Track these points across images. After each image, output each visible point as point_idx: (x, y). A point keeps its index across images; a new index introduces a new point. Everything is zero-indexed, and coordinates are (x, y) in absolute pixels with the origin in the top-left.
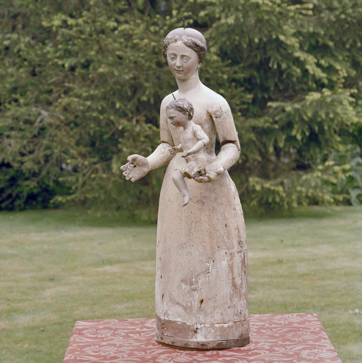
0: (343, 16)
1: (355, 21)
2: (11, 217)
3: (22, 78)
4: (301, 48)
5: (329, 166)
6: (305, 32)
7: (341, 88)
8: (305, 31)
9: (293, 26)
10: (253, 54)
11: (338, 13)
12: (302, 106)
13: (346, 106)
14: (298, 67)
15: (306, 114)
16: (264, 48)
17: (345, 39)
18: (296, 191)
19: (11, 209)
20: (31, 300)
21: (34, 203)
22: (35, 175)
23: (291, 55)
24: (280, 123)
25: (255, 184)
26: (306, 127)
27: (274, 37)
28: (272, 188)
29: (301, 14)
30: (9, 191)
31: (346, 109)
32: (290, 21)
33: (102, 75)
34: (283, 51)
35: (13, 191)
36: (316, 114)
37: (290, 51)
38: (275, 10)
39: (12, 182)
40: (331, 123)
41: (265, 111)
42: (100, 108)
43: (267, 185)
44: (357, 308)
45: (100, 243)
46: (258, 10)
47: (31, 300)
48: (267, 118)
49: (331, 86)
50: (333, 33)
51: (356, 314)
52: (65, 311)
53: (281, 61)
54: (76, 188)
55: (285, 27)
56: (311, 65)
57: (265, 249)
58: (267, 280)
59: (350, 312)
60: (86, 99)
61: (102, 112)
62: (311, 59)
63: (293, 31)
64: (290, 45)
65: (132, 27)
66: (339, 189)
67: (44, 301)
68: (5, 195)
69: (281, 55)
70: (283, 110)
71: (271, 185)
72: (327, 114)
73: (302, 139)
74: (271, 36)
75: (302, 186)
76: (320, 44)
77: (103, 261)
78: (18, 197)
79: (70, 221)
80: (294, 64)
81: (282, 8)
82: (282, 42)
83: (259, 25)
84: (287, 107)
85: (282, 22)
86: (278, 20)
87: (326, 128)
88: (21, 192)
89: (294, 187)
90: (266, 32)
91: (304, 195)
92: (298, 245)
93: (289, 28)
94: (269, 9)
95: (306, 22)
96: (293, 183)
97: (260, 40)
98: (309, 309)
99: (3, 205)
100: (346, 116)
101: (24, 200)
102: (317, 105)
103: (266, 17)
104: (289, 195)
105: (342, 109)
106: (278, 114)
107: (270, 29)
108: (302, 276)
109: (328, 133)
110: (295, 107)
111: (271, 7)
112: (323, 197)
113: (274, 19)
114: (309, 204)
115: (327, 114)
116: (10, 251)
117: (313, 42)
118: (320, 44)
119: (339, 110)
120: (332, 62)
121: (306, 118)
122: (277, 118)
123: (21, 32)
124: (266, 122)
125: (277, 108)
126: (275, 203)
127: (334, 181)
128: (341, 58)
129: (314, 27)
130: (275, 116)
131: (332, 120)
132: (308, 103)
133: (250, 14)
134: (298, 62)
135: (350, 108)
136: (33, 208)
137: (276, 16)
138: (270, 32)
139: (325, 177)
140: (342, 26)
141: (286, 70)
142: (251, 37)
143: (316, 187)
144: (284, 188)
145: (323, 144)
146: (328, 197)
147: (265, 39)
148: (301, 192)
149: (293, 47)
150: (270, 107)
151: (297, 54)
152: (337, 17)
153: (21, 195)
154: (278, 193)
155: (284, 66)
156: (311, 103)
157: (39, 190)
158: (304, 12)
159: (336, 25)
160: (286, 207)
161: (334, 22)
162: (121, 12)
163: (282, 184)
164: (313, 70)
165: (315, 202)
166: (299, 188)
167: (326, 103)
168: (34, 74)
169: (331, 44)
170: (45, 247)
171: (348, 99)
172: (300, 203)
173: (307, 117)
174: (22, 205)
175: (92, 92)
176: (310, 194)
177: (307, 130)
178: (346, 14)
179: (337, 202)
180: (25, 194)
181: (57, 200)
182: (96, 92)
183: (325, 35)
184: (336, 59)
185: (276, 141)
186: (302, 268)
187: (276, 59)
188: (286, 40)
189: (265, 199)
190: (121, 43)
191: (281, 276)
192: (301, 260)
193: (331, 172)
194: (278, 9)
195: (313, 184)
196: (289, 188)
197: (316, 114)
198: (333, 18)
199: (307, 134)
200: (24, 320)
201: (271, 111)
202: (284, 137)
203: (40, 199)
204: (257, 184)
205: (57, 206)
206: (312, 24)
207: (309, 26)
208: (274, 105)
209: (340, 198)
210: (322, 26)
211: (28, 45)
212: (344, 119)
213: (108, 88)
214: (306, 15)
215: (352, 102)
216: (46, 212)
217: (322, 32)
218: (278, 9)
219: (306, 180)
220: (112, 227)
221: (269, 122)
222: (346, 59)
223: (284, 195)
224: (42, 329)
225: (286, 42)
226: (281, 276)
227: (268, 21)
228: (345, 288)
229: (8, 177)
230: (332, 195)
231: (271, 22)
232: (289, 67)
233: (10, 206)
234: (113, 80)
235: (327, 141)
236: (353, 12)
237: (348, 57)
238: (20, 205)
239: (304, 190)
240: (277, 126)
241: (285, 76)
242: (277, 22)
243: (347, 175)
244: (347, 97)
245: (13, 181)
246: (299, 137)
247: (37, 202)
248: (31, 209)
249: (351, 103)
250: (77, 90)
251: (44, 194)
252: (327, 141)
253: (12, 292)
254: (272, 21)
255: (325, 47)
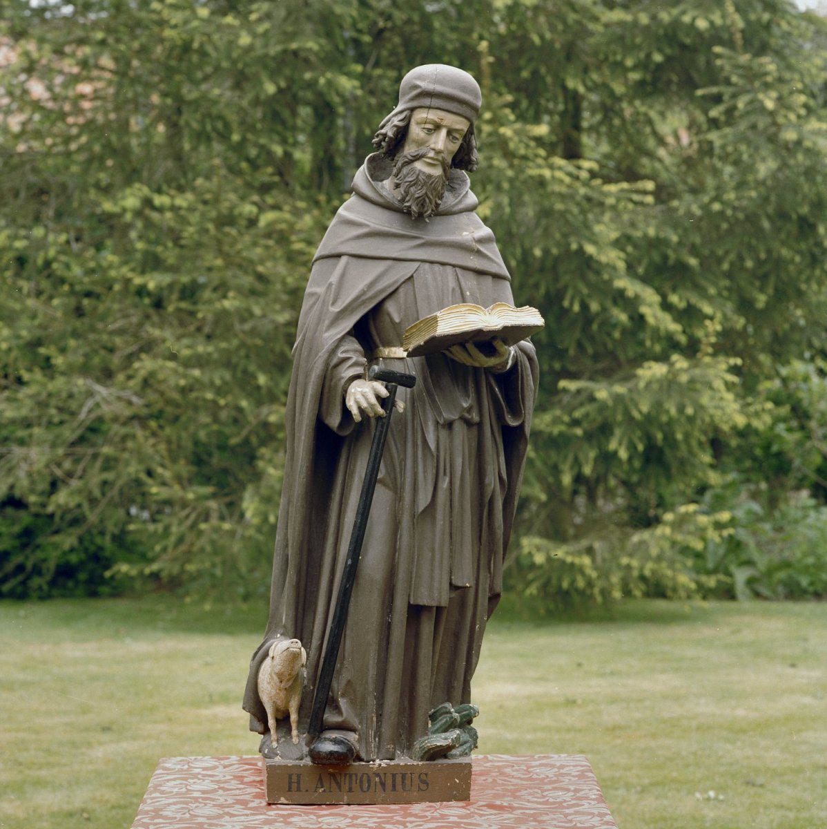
0: (716, 207)
1: (741, 216)
2: (22, 613)
3: (54, 319)
4: (631, 268)
5: (687, 514)
6: (639, 238)
7: (708, 354)
8: (638, 234)
9: (613, 226)
10: (531, 281)
11: (706, 199)
12: (630, 390)
13: (719, 391)
14: (625, 310)
15: (636, 406)
16: (554, 268)
17: (720, 252)
18: (619, 566)
19: (20, 596)
20: (65, 765)
21: (70, 584)
22: (76, 522)
23: (609, 283)
24: (585, 425)
25: (534, 551)
26: (639, 433)
27: (574, 246)
28: (569, 559)
29: (631, 200)
30: (17, 559)
31: (722, 399)
32: (607, 216)
33: (223, 315)
34: (592, 277)
35: (27, 558)
36: (658, 405)
37: (606, 277)
38: (577, 191)
39: (25, 540)
40: (688, 427)
41: (556, 399)
42: (218, 382)
43: (560, 552)
44: (712, 789)
45: (207, 664)
46: (541, 191)
47: (65, 765)
48: (558, 412)
49: (692, 350)
50: (698, 240)
51: (709, 799)
52: (134, 784)
53: (590, 296)
54: (165, 549)
55: (598, 228)
56: (650, 305)
57: (543, 679)
58: (539, 735)
59: (698, 795)
60: (188, 363)
61: (219, 391)
62: (650, 296)
63: (614, 235)
64: (608, 265)
65: (287, 216)
66: (710, 565)
67: (90, 767)
68: (9, 567)
69: (589, 284)
70: (592, 399)
71: (567, 553)
72: (681, 409)
73: (630, 459)
74: (569, 245)
75: (631, 555)
76: (671, 262)
77: (211, 696)
78: (37, 570)
79: (148, 621)
80: (615, 302)
81: (592, 188)
82: (590, 258)
83: (544, 222)
84: (599, 390)
85: (590, 216)
86: (583, 212)
87: (679, 436)
88: (44, 560)
89: (616, 558)
90: (558, 236)
91: (635, 573)
92: (612, 674)
93: (606, 230)
94: (564, 190)
95: (641, 218)
96: (612, 550)
97: (546, 252)
98: (617, 789)
99: (6, 588)
100: (719, 413)
101: (48, 578)
102: (661, 388)
103: (559, 206)
104: (604, 574)
105: (712, 398)
106: (582, 404)
107: (565, 230)
108: (614, 729)
109: (683, 447)
110: (616, 392)
111: (569, 186)
112: (674, 579)
113: (575, 210)
114: (647, 595)
115: (681, 409)
116: (21, 676)
117: (656, 257)
118: (671, 262)
119: (705, 400)
120: (695, 300)
121: (636, 414)
122: (577, 414)
123: (51, 225)
124: (556, 421)
125: (579, 392)
126: (577, 590)
127: (699, 546)
128: (712, 291)
129: (658, 228)
130: (574, 409)
131: (691, 420)
132: (642, 385)
133: (526, 198)
134: (619, 297)
135: (729, 396)
136: (67, 595)
137: (578, 204)
138: (565, 236)
139: (679, 537)
140: (718, 227)
141: (597, 314)
142: (527, 244)
143: (659, 559)
144: (594, 561)
145: (674, 471)
146: (685, 579)
147: (555, 251)
148: (628, 567)
149: (614, 268)
150: (565, 390)
151: (620, 283)
152: (705, 208)
153: (44, 566)
154: (581, 570)
155: (594, 306)
156: (649, 384)
157: (83, 556)
158: (636, 197)
159: (704, 224)
160: (599, 599)
161: (701, 219)
162: (265, 189)
163: (590, 551)
164: (656, 317)
165: (657, 590)
166: (625, 561)
167: (680, 384)
168: (79, 312)
169: (693, 262)
170: (93, 668)
171: (723, 379)
172: (627, 593)
173: (640, 412)
174: (45, 587)
175: (200, 349)
176: (647, 573)
177: (640, 439)
178: (723, 203)
179: (706, 593)
180: (52, 565)
181: (119, 571)
182: (210, 349)
183: (680, 243)
184: (704, 294)
185: (577, 463)
186: (613, 715)
187: (577, 292)
188: (598, 254)
189: (554, 582)
190: (267, 247)
191: (569, 730)
192: (614, 700)
193: (692, 528)
194: (582, 191)
195: (654, 551)
196: (604, 560)
197: (658, 405)
198: (697, 211)
199: (641, 447)
200: (48, 800)
201: (566, 399)
202: (592, 454)
203: (82, 576)
204: (537, 550)
205: (119, 590)
206: (653, 222)
207: (648, 225)
208: (572, 385)
209: (711, 582)
210: (675, 226)
211: (65, 249)
212: (717, 420)
213: (235, 342)
214: (641, 204)
215: (733, 384)
216: (92, 603)
217: (675, 238)
218: (582, 191)
219: (642, 543)
220: (231, 633)
221: (563, 423)
222: (725, 293)
223: (594, 574)
224: (85, 815)
225: (598, 258)
226: (569, 730)
227: (563, 214)
228: (695, 754)
229: (17, 529)
230: (694, 576)
231: (569, 217)
232: (604, 309)
233: (19, 589)
234: (247, 326)
235: (682, 463)
236: (738, 198)
237: (729, 289)
238: (40, 588)
239: (635, 563)
240: (579, 432)
241: (595, 327)
242: (581, 218)
243: (726, 533)
244: (721, 374)
245: (27, 537)
246: (623, 454)
247: (77, 582)
248: (63, 596)
249: (729, 386)
250: (171, 344)
251: (91, 566)
252: (682, 463)
253: (26, 749)
254: (571, 213)
255: (682, 267)
